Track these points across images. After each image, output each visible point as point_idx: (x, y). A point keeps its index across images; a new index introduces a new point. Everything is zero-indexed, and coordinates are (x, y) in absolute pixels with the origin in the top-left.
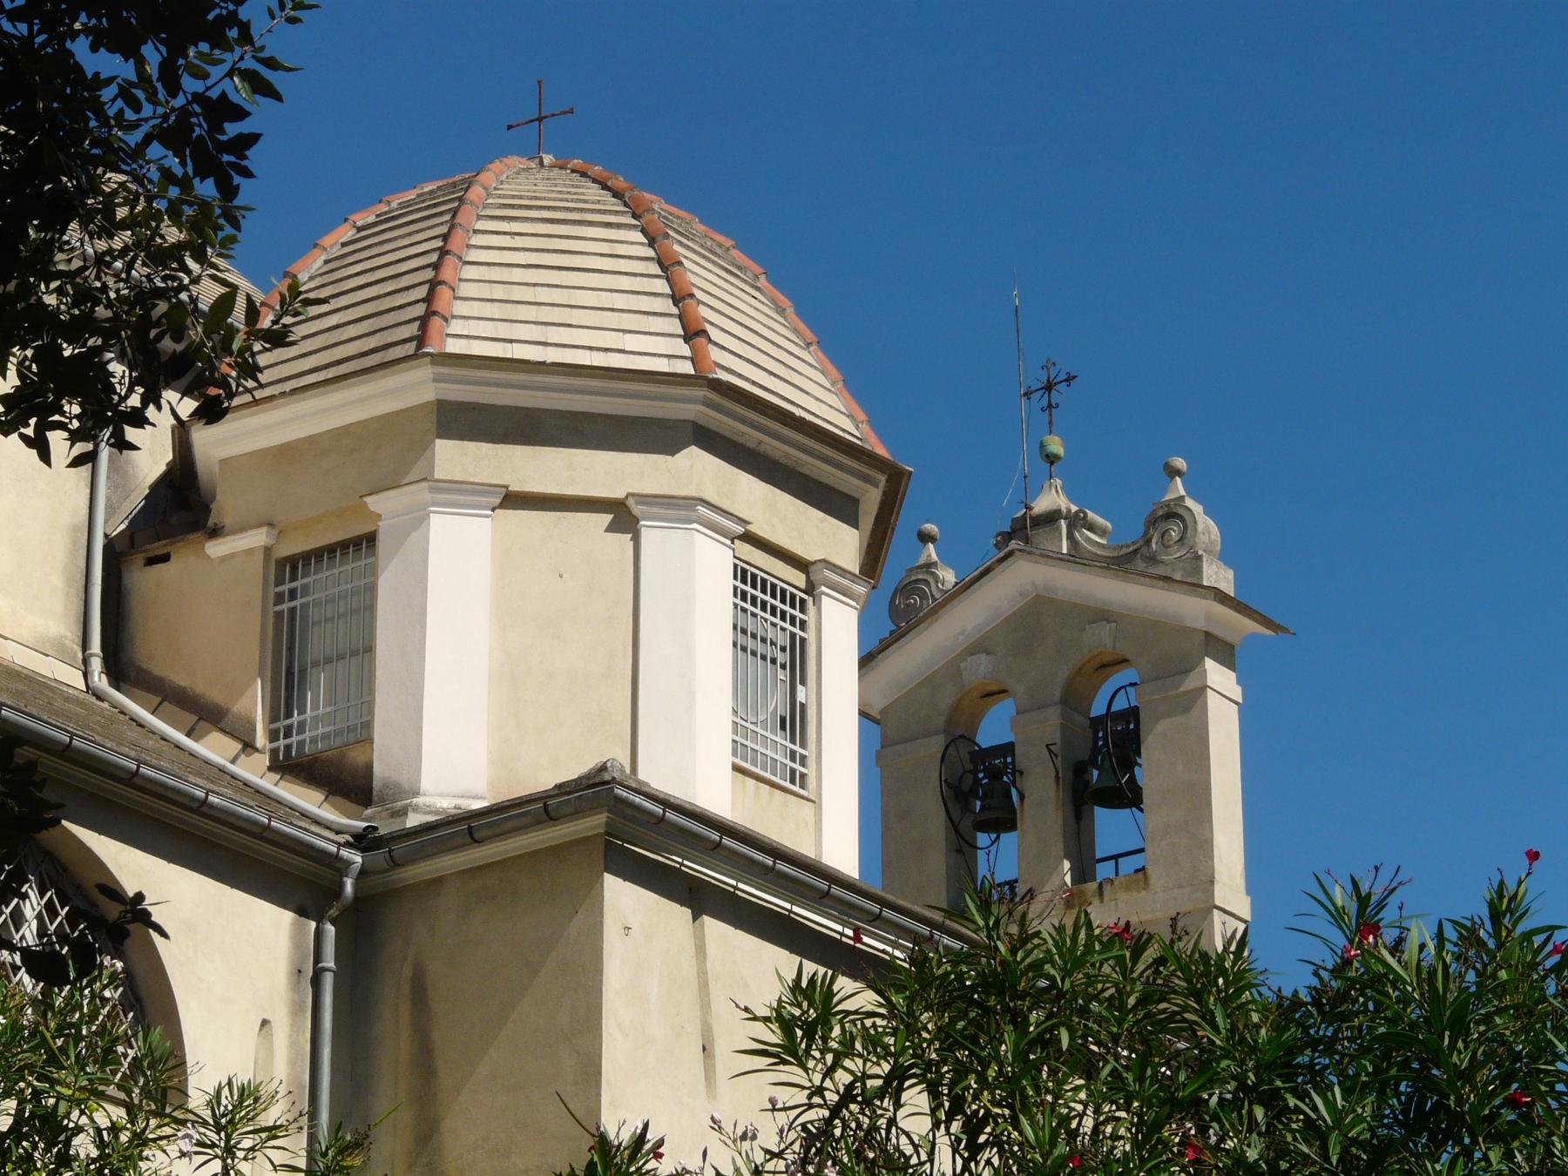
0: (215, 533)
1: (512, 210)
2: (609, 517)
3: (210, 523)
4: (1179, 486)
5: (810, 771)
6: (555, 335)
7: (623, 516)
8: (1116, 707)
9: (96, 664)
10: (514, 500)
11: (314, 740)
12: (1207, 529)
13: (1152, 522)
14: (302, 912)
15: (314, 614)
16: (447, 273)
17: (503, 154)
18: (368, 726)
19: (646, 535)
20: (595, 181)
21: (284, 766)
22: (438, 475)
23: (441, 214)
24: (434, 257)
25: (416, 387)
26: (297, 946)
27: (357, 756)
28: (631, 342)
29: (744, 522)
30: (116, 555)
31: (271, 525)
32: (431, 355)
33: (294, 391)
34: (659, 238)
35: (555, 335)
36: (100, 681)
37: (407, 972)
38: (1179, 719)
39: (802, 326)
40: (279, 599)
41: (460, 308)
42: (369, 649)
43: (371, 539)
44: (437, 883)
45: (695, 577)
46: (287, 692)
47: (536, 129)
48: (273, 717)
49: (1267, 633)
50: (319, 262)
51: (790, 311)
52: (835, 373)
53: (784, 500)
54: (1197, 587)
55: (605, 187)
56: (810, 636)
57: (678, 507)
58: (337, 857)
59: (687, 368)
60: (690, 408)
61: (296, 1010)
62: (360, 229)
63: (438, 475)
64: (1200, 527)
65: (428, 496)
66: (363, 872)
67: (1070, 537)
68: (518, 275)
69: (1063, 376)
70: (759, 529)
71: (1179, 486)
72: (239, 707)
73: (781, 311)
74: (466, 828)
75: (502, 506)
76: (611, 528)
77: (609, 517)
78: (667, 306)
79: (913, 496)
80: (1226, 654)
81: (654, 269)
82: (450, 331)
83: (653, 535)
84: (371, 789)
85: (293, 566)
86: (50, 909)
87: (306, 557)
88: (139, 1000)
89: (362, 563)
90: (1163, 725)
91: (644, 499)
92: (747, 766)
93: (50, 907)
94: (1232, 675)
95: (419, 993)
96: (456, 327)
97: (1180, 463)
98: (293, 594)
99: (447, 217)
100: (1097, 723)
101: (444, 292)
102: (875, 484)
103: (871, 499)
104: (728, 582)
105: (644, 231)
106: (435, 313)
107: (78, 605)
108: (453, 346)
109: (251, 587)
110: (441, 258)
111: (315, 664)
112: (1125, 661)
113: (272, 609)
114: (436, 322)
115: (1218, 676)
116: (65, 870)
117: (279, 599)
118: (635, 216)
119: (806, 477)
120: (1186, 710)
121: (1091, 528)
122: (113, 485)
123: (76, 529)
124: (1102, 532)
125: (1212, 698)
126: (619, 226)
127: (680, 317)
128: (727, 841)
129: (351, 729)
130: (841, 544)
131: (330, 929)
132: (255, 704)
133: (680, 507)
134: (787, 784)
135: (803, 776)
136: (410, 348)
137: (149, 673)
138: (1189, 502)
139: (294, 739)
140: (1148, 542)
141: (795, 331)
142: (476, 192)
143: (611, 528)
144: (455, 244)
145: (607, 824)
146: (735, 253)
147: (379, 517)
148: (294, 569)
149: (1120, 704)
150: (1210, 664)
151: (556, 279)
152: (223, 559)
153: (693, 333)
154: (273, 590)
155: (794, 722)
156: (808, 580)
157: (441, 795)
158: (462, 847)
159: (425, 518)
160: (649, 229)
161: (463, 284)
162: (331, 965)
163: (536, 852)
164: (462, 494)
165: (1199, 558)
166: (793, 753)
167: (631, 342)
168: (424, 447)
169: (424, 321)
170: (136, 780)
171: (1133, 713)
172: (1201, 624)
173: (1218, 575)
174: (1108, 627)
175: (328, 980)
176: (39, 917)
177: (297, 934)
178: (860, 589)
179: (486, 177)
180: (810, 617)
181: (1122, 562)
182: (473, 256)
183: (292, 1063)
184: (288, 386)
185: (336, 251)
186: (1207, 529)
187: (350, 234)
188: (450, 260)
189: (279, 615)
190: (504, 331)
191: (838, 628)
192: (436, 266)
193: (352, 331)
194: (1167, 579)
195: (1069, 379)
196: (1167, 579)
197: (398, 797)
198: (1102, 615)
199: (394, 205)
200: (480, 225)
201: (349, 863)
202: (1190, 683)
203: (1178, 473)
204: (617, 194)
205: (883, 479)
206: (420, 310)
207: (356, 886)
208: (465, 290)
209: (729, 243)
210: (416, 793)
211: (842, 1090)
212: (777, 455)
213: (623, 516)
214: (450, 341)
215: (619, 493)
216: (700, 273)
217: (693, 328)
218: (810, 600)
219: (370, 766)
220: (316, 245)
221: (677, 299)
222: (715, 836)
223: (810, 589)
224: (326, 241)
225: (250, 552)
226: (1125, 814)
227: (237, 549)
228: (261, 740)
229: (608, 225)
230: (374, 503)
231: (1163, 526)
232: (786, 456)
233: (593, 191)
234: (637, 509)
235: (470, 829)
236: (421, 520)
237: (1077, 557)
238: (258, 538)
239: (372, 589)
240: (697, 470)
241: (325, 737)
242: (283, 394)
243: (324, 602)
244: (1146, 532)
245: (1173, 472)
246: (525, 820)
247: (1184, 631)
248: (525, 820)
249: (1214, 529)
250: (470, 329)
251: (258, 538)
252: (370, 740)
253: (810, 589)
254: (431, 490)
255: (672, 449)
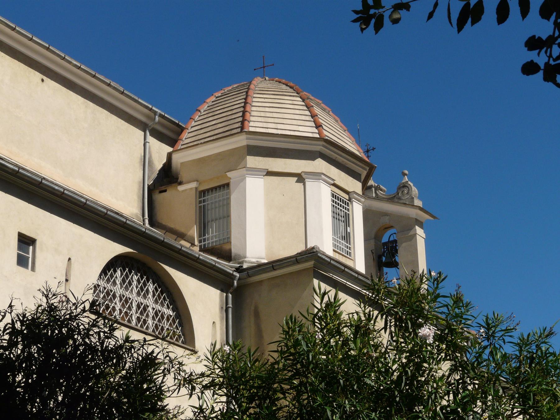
0: (181, 183)
1: (263, 91)
2: (296, 179)
3: (179, 181)
4: (406, 178)
5: (352, 251)
6: (280, 126)
7: (300, 178)
8: (390, 240)
9: (147, 221)
10: (270, 173)
11: (212, 242)
12: (415, 191)
13: (399, 188)
14: (222, 291)
15: (210, 207)
16: (248, 108)
17: (256, 77)
18: (229, 238)
19: (307, 183)
20: (283, 84)
21: (203, 249)
22: (248, 166)
23: (242, 93)
24: (243, 105)
25: (241, 141)
26: (221, 300)
27: (226, 247)
28: (301, 129)
29: (334, 180)
30: (151, 190)
31: (197, 181)
32: (246, 132)
33: (205, 143)
34: (306, 100)
35: (280, 126)
36: (147, 225)
37: (253, 308)
38: (409, 243)
39: (343, 125)
40: (200, 202)
41: (252, 119)
42: (229, 216)
43: (228, 185)
44: (261, 282)
45: (321, 196)
46: (203, 230)
47: (264, 69)
48: (200, 236)
49: (433, 218)
50: (206, 107)
51: (339, 121)
52: (352, 138)
53: (343, 174)
54: (413, 206)
55: (287, 85)
56: (350, 213)
57: (316, 175)
58: (232, 275)
59: (317, 136)
60: (319, 147)
61: (222, 319)
62: (217, 97)
63: (248, 166)
64: (413, 190)
65: (245, 172)
66: (239, 279)
67: (376, 193)
68: (267, 109)
69: (372, 148)
70: (337, 182)
71: (406, 178)
72: (190, 233)
73: (337, 121)
74: (260, 268)
75: (266, 175)
76: (297, 182)
77: (296, 179)
78: (310, 118)
79: (376, 173)
80: (421, 225)
81: (305, 108)
82: (250, 125)
83: (309, 184)
84: (231, 256)
85: (203, 193)
86: (156, 289)
87: (208, 190)
88: (180, 316)
89: (225, 192)
90: (404, 245)
91: (306, 173)
92: (336, 250)
93: (156, 288)
94: (423, 231)
95: (257, 315)
96: (251, 124)
97: (406, 172)
98: (204, 201)
99: (245, 93)
100: (384, 244)
101: (247, 114)
102: (366, 170)
103: (364, 174)
104: (330, 197)
105: (301, 98)
106: (246, 120)
107: (141, 204)
108: (251, 129)
109: (192, 199)
110: (245, 104)
111: (212, 221)
112: (392, 227)
113: (198, 205)
114: (246, 122)
115: (419, 231)
116: (159, 278)
117: (200, 202)
118: (297, 93)
119: (348, 168)
120: (410, 240)
121: (381, 190)
122: (149, 170)
123: (140, 182)
124: (384, 191)
125: (418, 237)
126: (293, 96)
127: (314, 122)
128: (346, 270)
129: (224, 239)
130: (355, 186)
131: (230, 295)
132: (194, 232)
133: (317, 176)
134: (346, 255)
135: (350, 253)
136: (239, 130)
137: (162, 224)
138: (409, 183)
139: (207, 242)
140: (398, 194)
141: (341, 127)
142: (252, 86)
143: (297, 182)
144: (249, 100)
145: (314, 264)
146: (322, 105)
147: (230, 178)
148: (204, 193)
149: (392, 239)
150: (417, 227)
151: (279, 112)
152: (183, 191)
153: (318, 126)
154: (198, 200)
155: (347, 237)
156: (349, 197)
157: (252, 258)
158: (271, 271)
159: (245, 178)
160: (302, 97)
161: (252, 112)
162: (231, 306)
163: (292, 273)
164: (255, 171)
165: (413, 198)
166: (347, 246)
167: (301, 129)
168: (243, 158)
169: (242, 123)
170: (180, 252)
171: (395, 241)
172: (414, 216)
173: (418, 203)
174: (387, 218)
175: (230, 310)
176: (153, 292)
177: (221, 296)
178: (363, 200)
179: (254, 82)
180: (350, 208)
181: (392, 199)
182: (254, 104)
183: (221, 334)
184: (202, 141)
185: (211, 104)
186: (415, 191)
187: (214, 99)
188: (248, 105)
189: (200, 207)
190: (265, 125)
191: (357, 211)
192: (244, 107)
193: (220, 125)
194: (405, 204)
195: (373, 149)
196: (405, 204)
197: (240, 259)
198: (386, 214)
199: (226, 91)
200: (255, 96)
201: (236, 276)
202: (411, 233)
203: (406, 175)
204: (291, 87)
205: (368, 168)
206: (241, 119)
207: (237, 283)
208: (253, 113)
209: (321, 102)
210: (245, 257)
211: (484, 325)
212: (341, 161)
213: (300, 178)
214: (250, 128)
215: (299, 171)
216: (317, 110)
217: (318, 124)
218: (350, 203)
219: (230, 250)
220: (205, 102)
221: (313, 116)
222: (343, 268)
223: (350, 200)
224: (208, 101)
225: (191, 189)
226: (393, 270)
227: (188, 187)
228: (196, 243)
229: (290, 96)
230: (229, 174)
231: (403, 189)
232: (343, 161)
233: (284, 87)
234: (304, 176)
235: (273, 266)
236: (243, 179)
237: (377, 198)
238: (194, 185)
239: (229, 199)
240: (320, 165)
241: (216, 241)
242: (201, 143)
243: (215, 201)
244: (398, 191)
245: (404, 174)
246: (290, 263)
247: (410, 218)
248: (290, 263)
249: (416, 190)
250: (255, 124)
251: (194, 185)
252: (231, 243)
253: (350, 200)
254: (247, 170)
255: (314, 159)
